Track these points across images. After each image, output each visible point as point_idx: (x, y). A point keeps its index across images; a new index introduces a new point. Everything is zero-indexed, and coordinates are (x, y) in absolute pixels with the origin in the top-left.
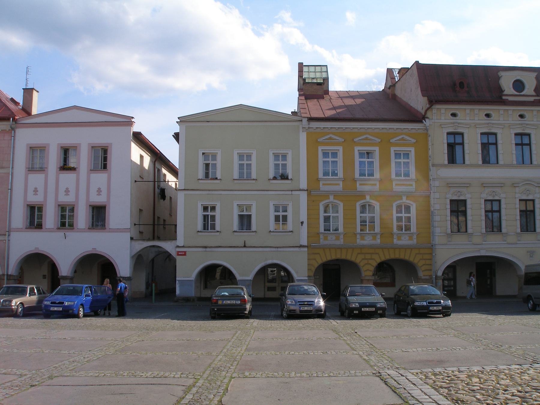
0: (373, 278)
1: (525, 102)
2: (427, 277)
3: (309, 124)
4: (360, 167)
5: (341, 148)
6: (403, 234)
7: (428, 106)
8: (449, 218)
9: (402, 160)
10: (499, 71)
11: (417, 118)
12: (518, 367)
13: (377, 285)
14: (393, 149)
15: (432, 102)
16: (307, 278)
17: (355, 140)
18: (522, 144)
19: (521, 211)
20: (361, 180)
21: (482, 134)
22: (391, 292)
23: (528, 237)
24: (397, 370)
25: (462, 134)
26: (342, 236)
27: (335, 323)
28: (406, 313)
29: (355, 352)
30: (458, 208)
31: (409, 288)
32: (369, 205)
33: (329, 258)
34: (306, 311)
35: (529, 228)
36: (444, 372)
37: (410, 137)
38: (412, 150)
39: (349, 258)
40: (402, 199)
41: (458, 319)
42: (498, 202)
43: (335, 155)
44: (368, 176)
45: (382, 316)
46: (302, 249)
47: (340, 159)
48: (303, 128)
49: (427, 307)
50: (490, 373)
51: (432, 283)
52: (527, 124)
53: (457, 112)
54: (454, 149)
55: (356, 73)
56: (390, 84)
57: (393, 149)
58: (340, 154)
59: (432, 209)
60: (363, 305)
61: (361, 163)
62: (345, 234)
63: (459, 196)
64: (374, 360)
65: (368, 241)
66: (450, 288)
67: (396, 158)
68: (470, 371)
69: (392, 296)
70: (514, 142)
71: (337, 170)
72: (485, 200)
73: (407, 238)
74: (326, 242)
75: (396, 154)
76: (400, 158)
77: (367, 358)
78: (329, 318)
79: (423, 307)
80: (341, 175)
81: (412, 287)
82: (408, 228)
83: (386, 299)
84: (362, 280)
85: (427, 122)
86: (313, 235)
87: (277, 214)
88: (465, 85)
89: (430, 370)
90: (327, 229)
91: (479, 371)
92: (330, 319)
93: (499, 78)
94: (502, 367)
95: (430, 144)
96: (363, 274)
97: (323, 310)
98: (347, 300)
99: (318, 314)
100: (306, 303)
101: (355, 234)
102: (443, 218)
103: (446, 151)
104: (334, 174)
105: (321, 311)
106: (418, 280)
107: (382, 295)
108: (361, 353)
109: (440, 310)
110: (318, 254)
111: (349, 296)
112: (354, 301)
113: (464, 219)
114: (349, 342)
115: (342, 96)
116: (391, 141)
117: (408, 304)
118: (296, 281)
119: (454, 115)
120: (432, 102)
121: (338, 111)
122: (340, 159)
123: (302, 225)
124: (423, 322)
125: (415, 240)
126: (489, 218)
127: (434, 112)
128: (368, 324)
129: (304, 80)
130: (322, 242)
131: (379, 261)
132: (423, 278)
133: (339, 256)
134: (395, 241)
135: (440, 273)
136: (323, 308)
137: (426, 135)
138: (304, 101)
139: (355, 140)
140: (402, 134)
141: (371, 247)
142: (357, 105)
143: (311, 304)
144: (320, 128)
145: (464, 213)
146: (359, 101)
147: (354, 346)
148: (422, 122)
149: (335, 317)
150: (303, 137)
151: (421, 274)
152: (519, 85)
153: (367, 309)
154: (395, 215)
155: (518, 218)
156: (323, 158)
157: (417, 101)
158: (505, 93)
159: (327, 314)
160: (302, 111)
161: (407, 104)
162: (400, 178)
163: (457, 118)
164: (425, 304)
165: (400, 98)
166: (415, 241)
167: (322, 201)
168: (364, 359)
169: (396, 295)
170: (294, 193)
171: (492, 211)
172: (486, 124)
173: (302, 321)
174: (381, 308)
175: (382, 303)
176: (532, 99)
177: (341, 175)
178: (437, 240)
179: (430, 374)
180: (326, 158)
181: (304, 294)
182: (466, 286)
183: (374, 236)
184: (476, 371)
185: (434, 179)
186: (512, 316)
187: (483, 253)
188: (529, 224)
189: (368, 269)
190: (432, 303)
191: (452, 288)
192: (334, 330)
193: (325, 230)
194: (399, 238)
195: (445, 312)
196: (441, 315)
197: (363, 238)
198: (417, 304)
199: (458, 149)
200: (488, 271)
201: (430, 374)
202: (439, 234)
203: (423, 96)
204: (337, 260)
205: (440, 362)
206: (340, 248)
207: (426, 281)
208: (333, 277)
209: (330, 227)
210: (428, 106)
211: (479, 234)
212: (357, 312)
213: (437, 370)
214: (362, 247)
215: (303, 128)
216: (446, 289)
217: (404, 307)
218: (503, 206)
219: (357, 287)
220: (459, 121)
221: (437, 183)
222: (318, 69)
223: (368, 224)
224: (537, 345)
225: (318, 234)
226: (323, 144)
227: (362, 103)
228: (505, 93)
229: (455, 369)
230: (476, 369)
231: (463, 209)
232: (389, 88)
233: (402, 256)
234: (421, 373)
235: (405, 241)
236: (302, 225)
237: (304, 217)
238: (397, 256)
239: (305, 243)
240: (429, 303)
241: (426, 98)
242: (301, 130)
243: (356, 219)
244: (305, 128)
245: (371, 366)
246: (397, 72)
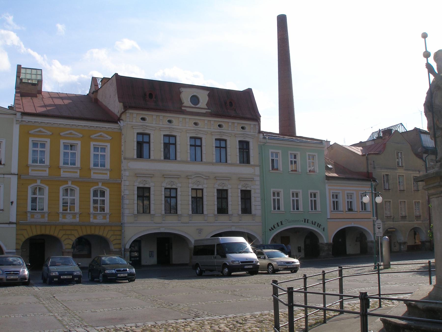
0: (72, 250)
1: (199, 113)
2: (117, 250)
3: (22, 118)
4: (64, 157)
5: (48, 140)
6: (98, 214)
7: (123, 110)
8: (136, 202)
9: (100, 153)
10: (180, 87)
11: (112, 119)
12: (183, 320)
13: (74, 256)
14: (92, 143)
15: (126, 108)
16: (15, 251)
17: (62, 134)
18: (195, 146)
19: (192, 197)
20: (95, 169)
21: (164, 135)
22: (86, 262)
23: (198, 218)
24: (86, 328)
25: (149, 135)
26: (46, 215)
27: (38, 290)
28: (98, 280)
29: (51, 314)
30: (144, 194)
31: (101, 259)
32: (40, 188)
33: (35, 234)
34: (12, 279)
35: (198, 211)
36: (124, 328)
37: (106, 134)
38: (109, 145)
39: (52, 233)
40: (98, 185)
41: (140, 284)
42: (175, 190)
43: (43, 145)
44: (40, 163)
45: (78, 282)
46: (11, 226)
47: (47, 149)
48: (17, 120)
49: (115, 274)
50: (161, 327)
51: (122, 255)
52: (200, 130)
53: (146, 117)
54: (142, 148)
55: (64, 78)
56: (93, 90)
57: (92, 143)
58: (48, 145)
59: (123, 194)
60: (62, 273)
61: (65, 154)
62: (49, 213)
63: (144, 185)
64: (66, 320)
65: (69, 219)
66: (136, 259)
67: (94, 151)
68: (145, 326)
69: (87, 265)
70: (214, 145)
71: (44, 158)
72: (165, 188)
73: (102, 217)
74: (33, 220)
75: (95, 148)
76: (98, 151)
77: (60, 318)
78: (32, 285)
79: (112, 274)
80: (47, 162)
81: (103, 258)
82: (103, 209)
83: (82, 268)
84: (63, 252)
85: (122, 123)
86: (22, 213)
89: (113, 326)
90: (34, 209)
91: (152, 325)
92: (33, 286)
93: (180, 93)
94: (170, 322)
95: (123, 141)
96: (64, 247)
97: (28, 278)
98: (48, 269)
99: (24, 282)
100: (12, 272)
101: (58, 214)
102: (131, 202)
103: (136, 148)
104: (42, 162)
105: (26, 279)
106: (110, 252)
107: (78, 265)
108: (56, 314)
109: (126, 277)
111: (50, 266)
112: (54, 270)
113: (148, 203)
114: (47, 305)
115: (52, 96)
116: (91, 137)
117: (100, 272)
118: (5, 253)
119: (143, 119)
120: (126, 108)
121: (48, 108)
122: (47, 149)
123: (12, 205)
124: (112, 286)
125: (108, 219)
126: (168, 202)
127: (127, 115)
128: (66, 289)
129: (21, 80)
130: (30, 219)
131: (77, 236)
132: (114, 250)
133: (43, 232)
134: (92, 220)
135: (128, 247)
136: (27, 277)
137: (120, 133)
138: (20, 98)
139: (62, 134)
140: (100, 131)
141: (71, 224)
142: (66, 105)
143: (16, 273)
144: (38, 122)
145: (149, 198)
146: (67, 102)
147: (50, 309)
148: (117, 123)
149: (38, 284)
150: (16, 129)
151: (112, 247)
152: (195, 100)
153: (65, 277)
154: (92, 198)
155: (190, 203)
156: (33, 147)
157: (114, 105)
158: (184, 105)
159: (31, 281)
160: (17, 106)
161: (106, 107)
162: (97, 168)
163: (146, 122)
164: (114, 271)
165: (101, 103)
166: (108, 220)
167: (93, 186)
168: (59, 320)
169: (90, 265)
170: (6, 176)
171: (170, 197)
172: (141, 125)
173: (8, 288)
174: (76, 276)
175: (78, 272)
176: (204, 111)
177: (47, 162)
178: (126, 219)
179: (112, 330)
180: (35, 147)
181: (10, 265)
182: (149, 257)
183: (74, 215)
184: (150, 325)
185: (125, 170)
186: (183, 280)
187: (162, 230)
188: (198, 208)
189: (68, 243)
190: (120, 271)
191: (138, 259)
192: (36, 296)
193: (32, 209)
194: (95, 217)
195: (131, 278)
196: (127, 281)
197: (95, 217)
198: (107, 272)
199: (145, 146)
200: (167, 244)
201: (112, 330)
202: (128, 215)
203: (120, 102)
204: (42, 235)
205: (122, 320)
206: (44, 225)
207: (115, 253)
208: (37, 250)
209: (36, 206)
210: (123, 110)
211: (160, 215)
212: (57, 279)
213: (118, 326)
214: (64, 224)
215: (17, 120)
216: (132, 259)
217: (97, 275)
218: (179, 193)
219: (57, 258)
220: (148, 124)
221: (127, 173)
222: (34, 72)
223: (69, 205)
224: (199, 303)
225: (26, 212)
226: (34, 135)
227: (69, 103)
228: (184, 105)
229: (133, 325)
230: (149, 324)
231: (147, 194)
232: (93, 93)
233: (97, 232)
234: (105, 329)
235: (99, 220)
236: (12, 205)
237: (14, 197)
238: (93, 232)
239: (14, 220)
240: (117, 271)
241: (122, 104)
242: (15, 122)
243: (59, 200)
244: (18, 120)
245: (64, 325)
246: (100, 81)
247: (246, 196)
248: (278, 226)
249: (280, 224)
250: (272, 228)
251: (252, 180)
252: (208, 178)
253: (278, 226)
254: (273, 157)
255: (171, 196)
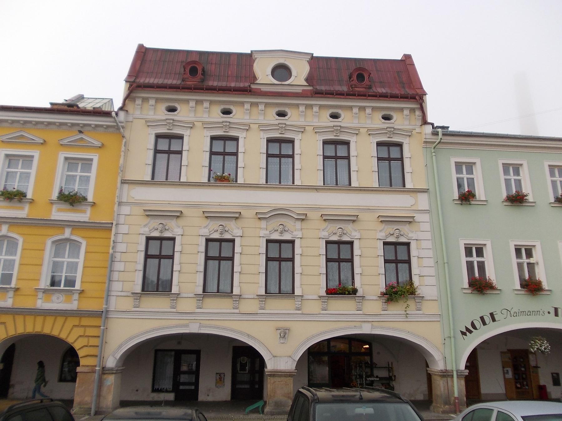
23: (278, 306)
72: (268, 241)
81: (456, 395)
87: (480, 259)
88: (200, 71)
110: (4, 323)
135: (111, 363)
152: (281, 71)
158: (258, 82)
163: (340, 120)
171: (160, 257)
178: (115, 304)
202: (120, 294)
221: (126, 210)
247: (398, 255)
248: (484, 323)
249: (488, 319)
250: (467, 329)
251: (410, 221)
252: (303, 219)
253: (484, 323)
254: (509, 175)
255: (219, 253)
